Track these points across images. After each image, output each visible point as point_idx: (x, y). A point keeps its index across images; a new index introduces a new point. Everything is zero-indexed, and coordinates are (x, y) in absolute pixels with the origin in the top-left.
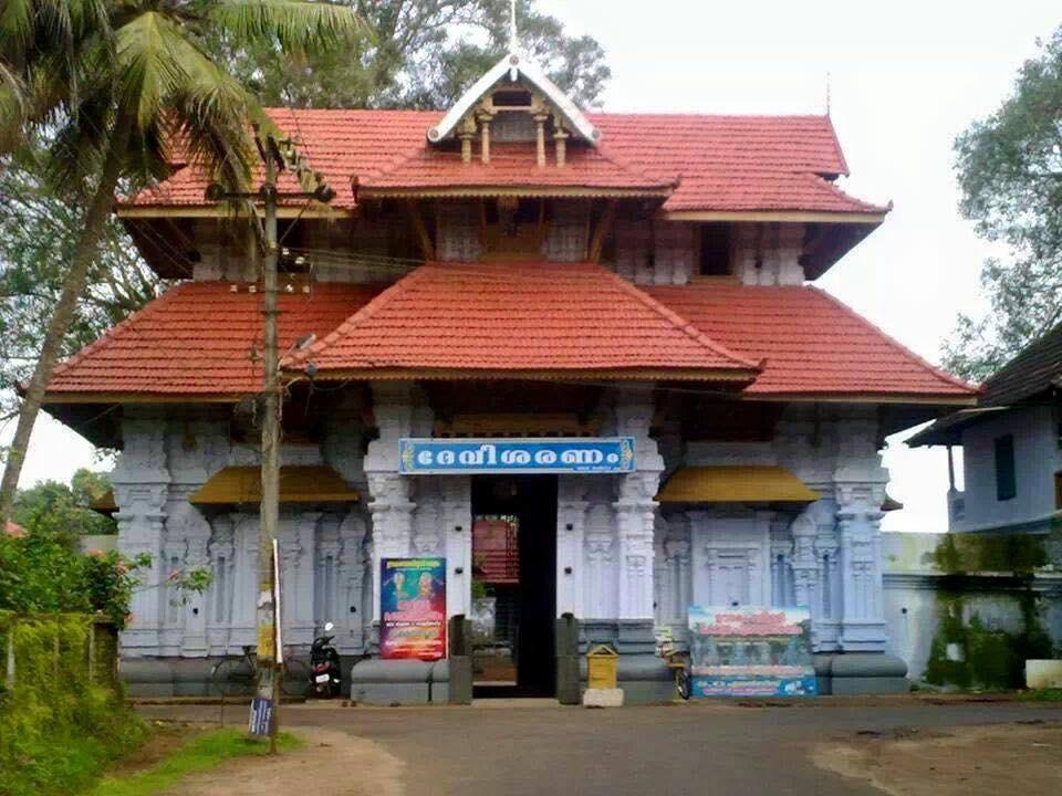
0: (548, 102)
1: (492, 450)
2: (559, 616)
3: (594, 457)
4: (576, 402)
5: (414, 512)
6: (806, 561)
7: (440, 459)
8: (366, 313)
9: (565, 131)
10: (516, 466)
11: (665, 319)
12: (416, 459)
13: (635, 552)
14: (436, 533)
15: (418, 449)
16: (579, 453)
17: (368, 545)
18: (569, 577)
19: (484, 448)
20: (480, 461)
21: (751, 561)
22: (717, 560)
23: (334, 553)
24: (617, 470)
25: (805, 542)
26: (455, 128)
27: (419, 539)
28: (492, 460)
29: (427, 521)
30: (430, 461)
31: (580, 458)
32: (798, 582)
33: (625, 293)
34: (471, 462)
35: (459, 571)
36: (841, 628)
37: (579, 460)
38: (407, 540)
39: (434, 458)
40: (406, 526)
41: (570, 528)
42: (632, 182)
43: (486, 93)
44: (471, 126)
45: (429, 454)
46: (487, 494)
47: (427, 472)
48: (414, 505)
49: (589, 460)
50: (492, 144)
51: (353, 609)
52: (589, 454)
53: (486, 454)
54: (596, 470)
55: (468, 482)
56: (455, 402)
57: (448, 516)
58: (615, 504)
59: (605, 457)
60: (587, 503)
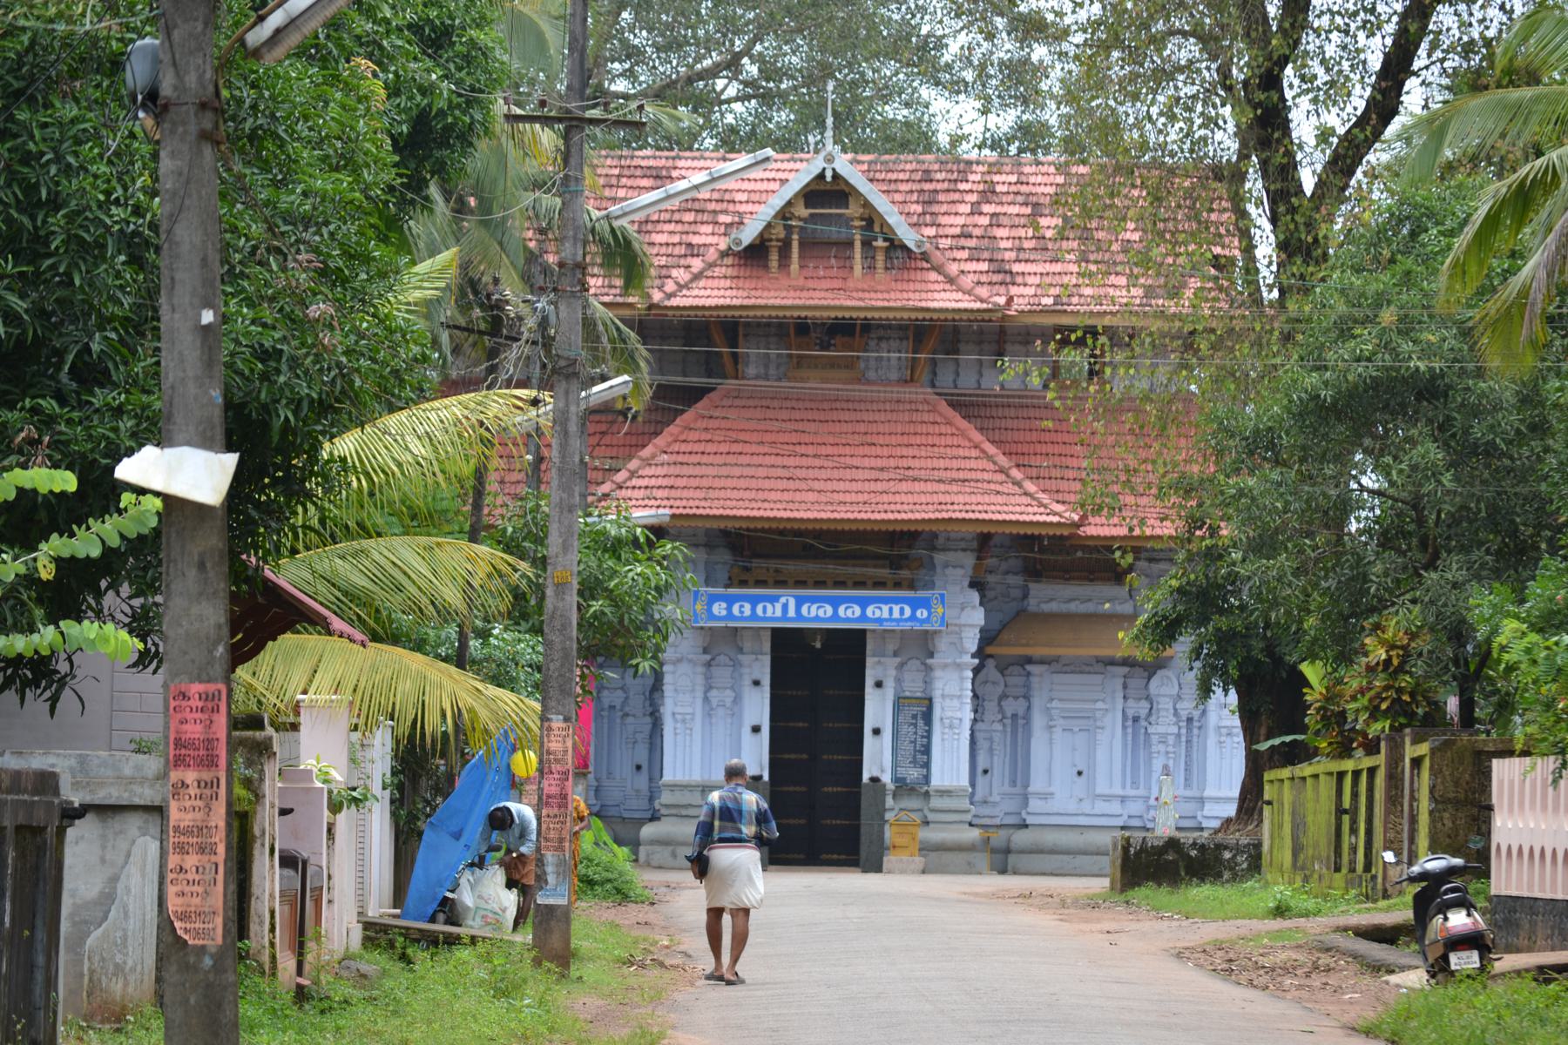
0: (867, 204)
1: (792, 602)
2: (866, 777)
3: (902, 611)
4: (892, 554)
5: (708, 665)
6: (1165, 725)
7: (736, 610)
8: (655, 446)
9: (885, 240)
10: (848, 620)
11: (990, 458)
12: (709, 610)
13: (950, 714)
14: (732, 688)
15: (713, 599)
16: (885, 608)
17: (656, 695)
18: (878, 691)
19: (783, 600)
20: (779, 613)
21: (1099, 724)
22: (1061, 721)
23: (618, 703)
24: (926, 627)
25: (1165, 704)
26: (761, 234)
27: (714, 693)
28: (792, 613)
29: (722, 674)
30: (724, 613)
31: (882, 612)
32: (1154, 749)
33: (949, 423)
34: (769, 613)
35: (756, 729)
36: (1201, 801)
37: (886, 615)
38: (699, 694)
39: (729, 609)
40: (700, 680)
41: (879, 685)
42: (877, 732)
43: (796, 195)
44: (779, 232)
45: (724, 605)
46: (790, 649)
47: (722, 624)
48: (708, 657)
49: (896, 614)
50: (801, 244)
51: (639, 768)
52: (896, 609)
53: (785, 607)
54: (907, 626)
55: (769, 633)
56: (754, 551)
57: (746, 670)
58: (929, 661)
59: (914, 612)
60: (898, 660)
